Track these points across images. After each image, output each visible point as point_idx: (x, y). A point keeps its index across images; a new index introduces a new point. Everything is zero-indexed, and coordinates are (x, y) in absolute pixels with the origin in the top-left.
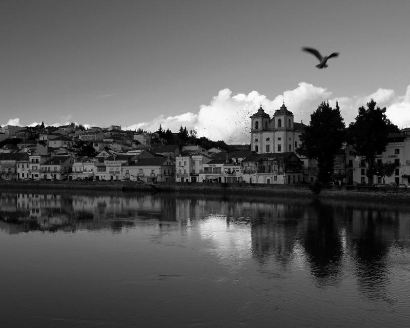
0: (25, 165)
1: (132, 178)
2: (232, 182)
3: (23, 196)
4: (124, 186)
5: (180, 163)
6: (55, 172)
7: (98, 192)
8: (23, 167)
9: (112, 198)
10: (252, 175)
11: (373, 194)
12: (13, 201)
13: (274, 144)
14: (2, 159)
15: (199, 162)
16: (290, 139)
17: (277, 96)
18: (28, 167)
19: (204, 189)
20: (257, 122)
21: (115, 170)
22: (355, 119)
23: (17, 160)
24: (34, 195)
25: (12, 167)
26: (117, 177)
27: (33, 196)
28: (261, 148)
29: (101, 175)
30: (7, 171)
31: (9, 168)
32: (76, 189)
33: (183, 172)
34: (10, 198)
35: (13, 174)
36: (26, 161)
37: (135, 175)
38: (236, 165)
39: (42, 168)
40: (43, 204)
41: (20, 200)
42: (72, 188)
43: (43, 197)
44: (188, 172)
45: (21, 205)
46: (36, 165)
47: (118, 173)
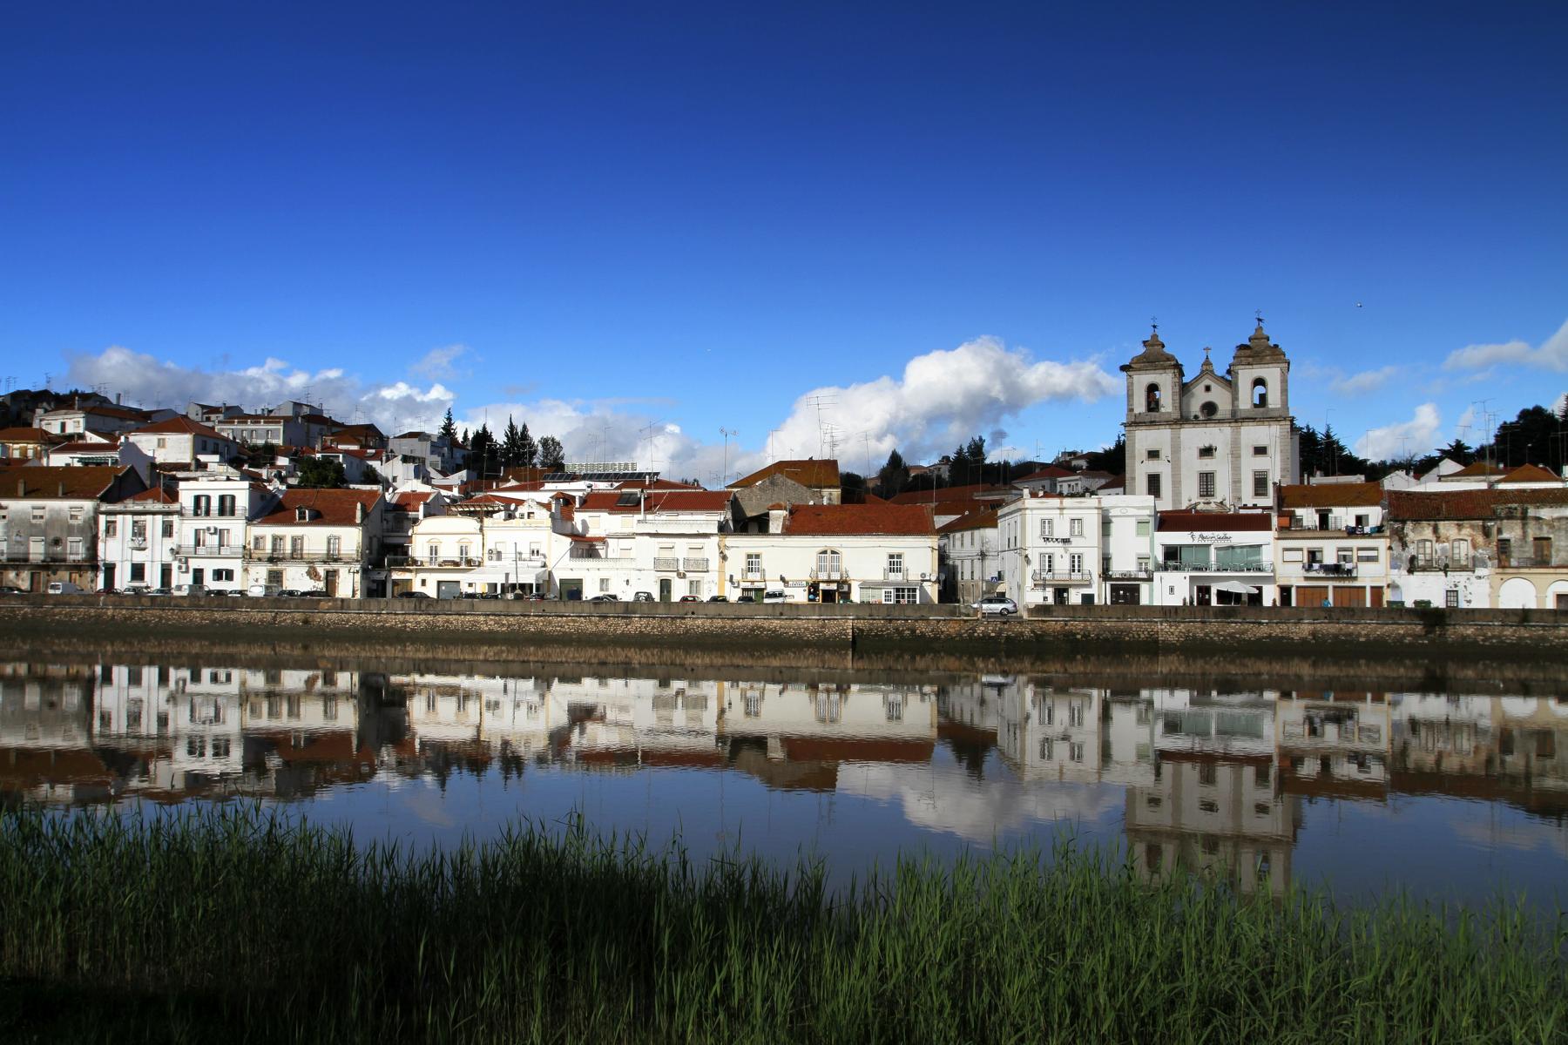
0: (154, 524)
2: (1368, 605)
3: (135, 679)
4: (860, 624)
5: (1046, 523)
6: (332, 558)
8: (139, 531)
9: (664, 683)
12: (72, 698)
13: (1236, 469)
14: (12, 495)
15: (1133, 521)
17: (912, 358)
18: (168, 531)
19: (1314, 634)
20: (1152, 388)
23: (104, 499)
24: (206, 673)
25: (70, 530)
28: (1176, 483)
29: (592, 578)
30: (37, 550)
31: (55, 535)
32: (565, 640)
33: (1062, 565)
34: (49, 684)
35: (77, 567)
36: (158, 506)
40: (255, 712)
41: (112, 698)
42: (541, 640)
43: (257, 680)
44: (1092, 565)
45: (119, 725)
46: (222, 523)
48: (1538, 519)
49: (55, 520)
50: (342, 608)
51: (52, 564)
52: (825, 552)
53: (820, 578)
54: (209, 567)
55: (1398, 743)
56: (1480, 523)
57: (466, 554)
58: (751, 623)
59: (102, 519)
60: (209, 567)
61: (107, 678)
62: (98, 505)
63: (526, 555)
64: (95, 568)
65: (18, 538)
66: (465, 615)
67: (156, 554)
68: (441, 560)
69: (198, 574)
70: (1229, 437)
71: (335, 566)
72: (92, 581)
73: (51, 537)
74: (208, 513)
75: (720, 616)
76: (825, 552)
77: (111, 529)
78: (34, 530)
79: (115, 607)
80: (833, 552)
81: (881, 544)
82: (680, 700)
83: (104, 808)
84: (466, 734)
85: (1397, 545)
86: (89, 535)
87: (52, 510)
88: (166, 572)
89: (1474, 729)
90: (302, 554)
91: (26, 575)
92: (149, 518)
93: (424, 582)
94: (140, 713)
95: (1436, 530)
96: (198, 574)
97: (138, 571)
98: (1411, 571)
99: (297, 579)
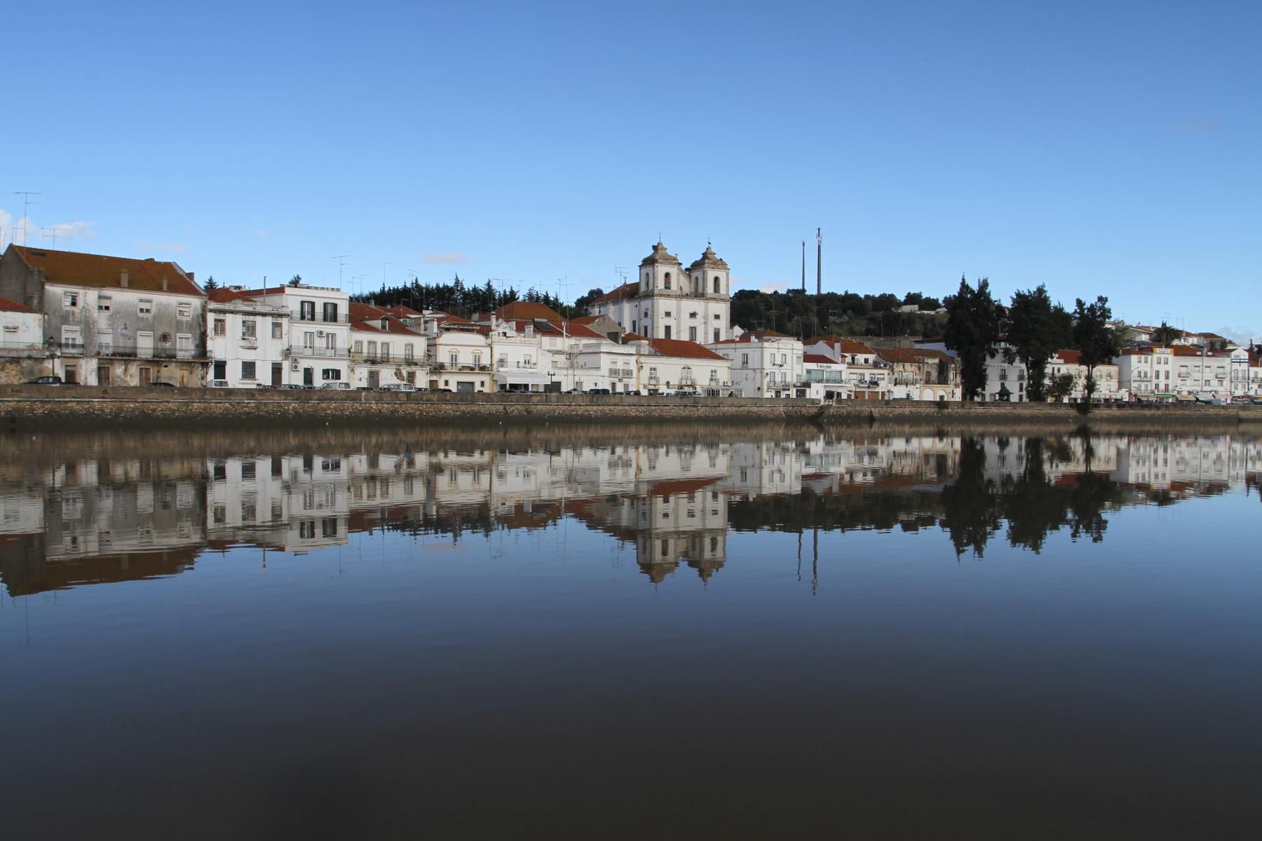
1: (663, 389)
2: (880, 398)
3: (249, 471)
6: (410, 362)
7: (726, 431)
10: (911, 388)
11: (1147, 412)
12: (185, 496)
16: (646, 315)
21: (620, 366)
22: (1080, 303)
24: (318, 462)
25: (179, 326)
26: (626, 386)
27: (308, 465)
30: (146, 345)
34: (163, 485)
37: (675, 381)
38: (881, 368)
39: (359, 343)
46: (328, 328)
47: (628, 373)
48: (927, 363)
49: (162, 315)
50: (546, 401)
51: (162, 358)
52: (684, 368)
53: (683, 384)
54: (318, 367)
55: (890, 464)
56: (917, 364)
57: (479, 361)
58: (746, 409)
59: (211, 318)
60: (318, 367)
61: (221, 473)
62: (206, 302)
63: (522, 364)
64: (205, 365)
65: (125, 332)
66: (618, 405)
67: (267, 352)
68: (460, 365)
69: (308, 374)
70: (703, 307)
71: (413, 368)
72: (202, 378)
73: (160, 332)
74: (313, 318)
75: (732, 405)
76: (684, 368)
77: (220, 327)
78: (141, 325)
79: (378, 402)
80: (689, 368)
81: (706, 364)
82: (620, 462)
83: (722, 537)
84: (477, 498)
85: (891, 373)
86: (198, 332)
87: (159, 304)
88: (277, 370)
89: (913, 454)
90: (388, 358)
91: (134, 369)
92: (259, 319)
93: (447, 383)
94: (648, 481)
95: (904, 367)
96: (308, 374)
97: (249, 369)
98: (895, 385)
99: (387, 377)
